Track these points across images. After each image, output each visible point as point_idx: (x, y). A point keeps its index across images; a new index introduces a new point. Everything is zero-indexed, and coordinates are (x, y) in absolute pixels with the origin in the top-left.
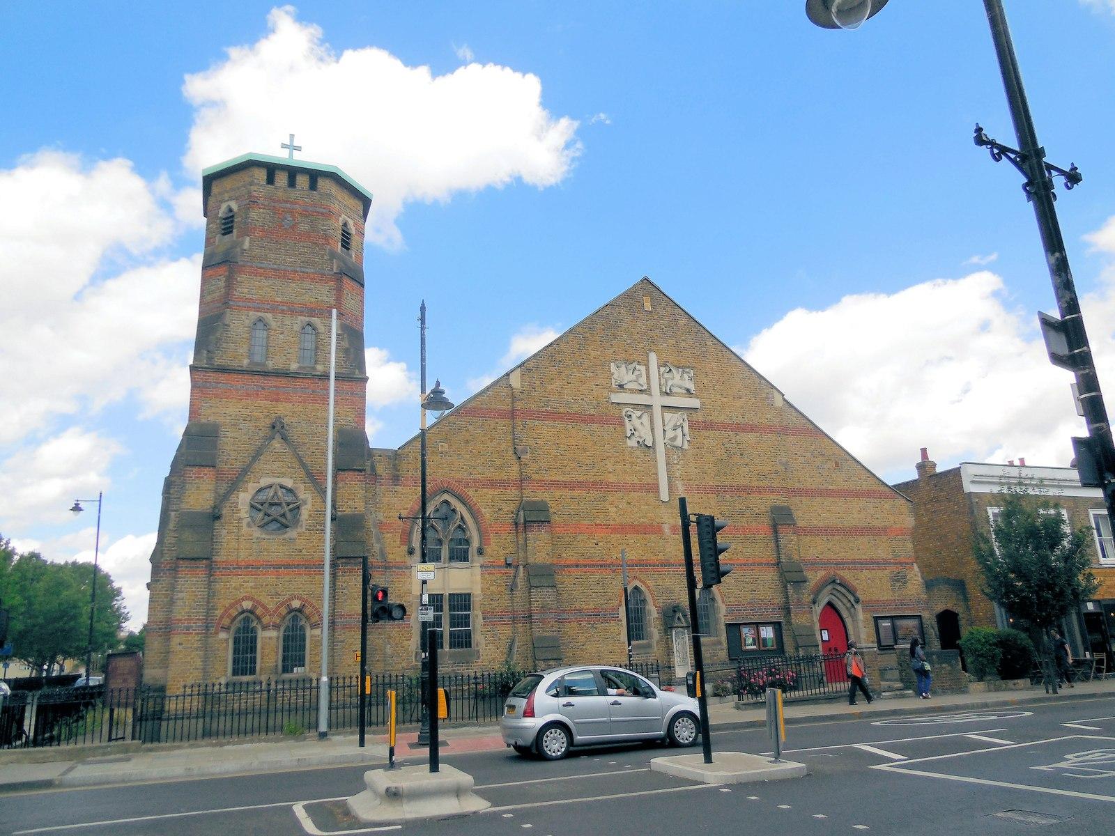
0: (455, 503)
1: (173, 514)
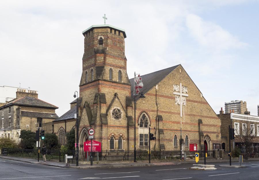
0: (145, 114)
1: (98, 114)
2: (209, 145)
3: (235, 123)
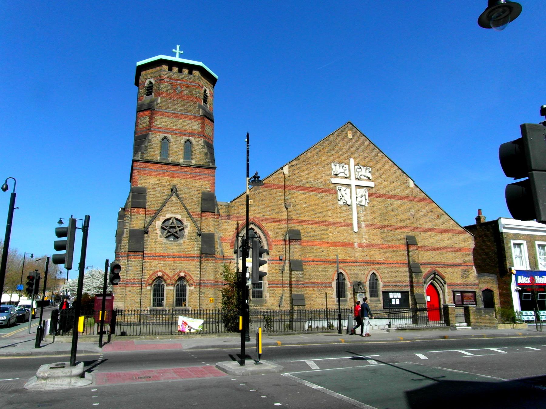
2: (444, 295)
3: (512, 241)
